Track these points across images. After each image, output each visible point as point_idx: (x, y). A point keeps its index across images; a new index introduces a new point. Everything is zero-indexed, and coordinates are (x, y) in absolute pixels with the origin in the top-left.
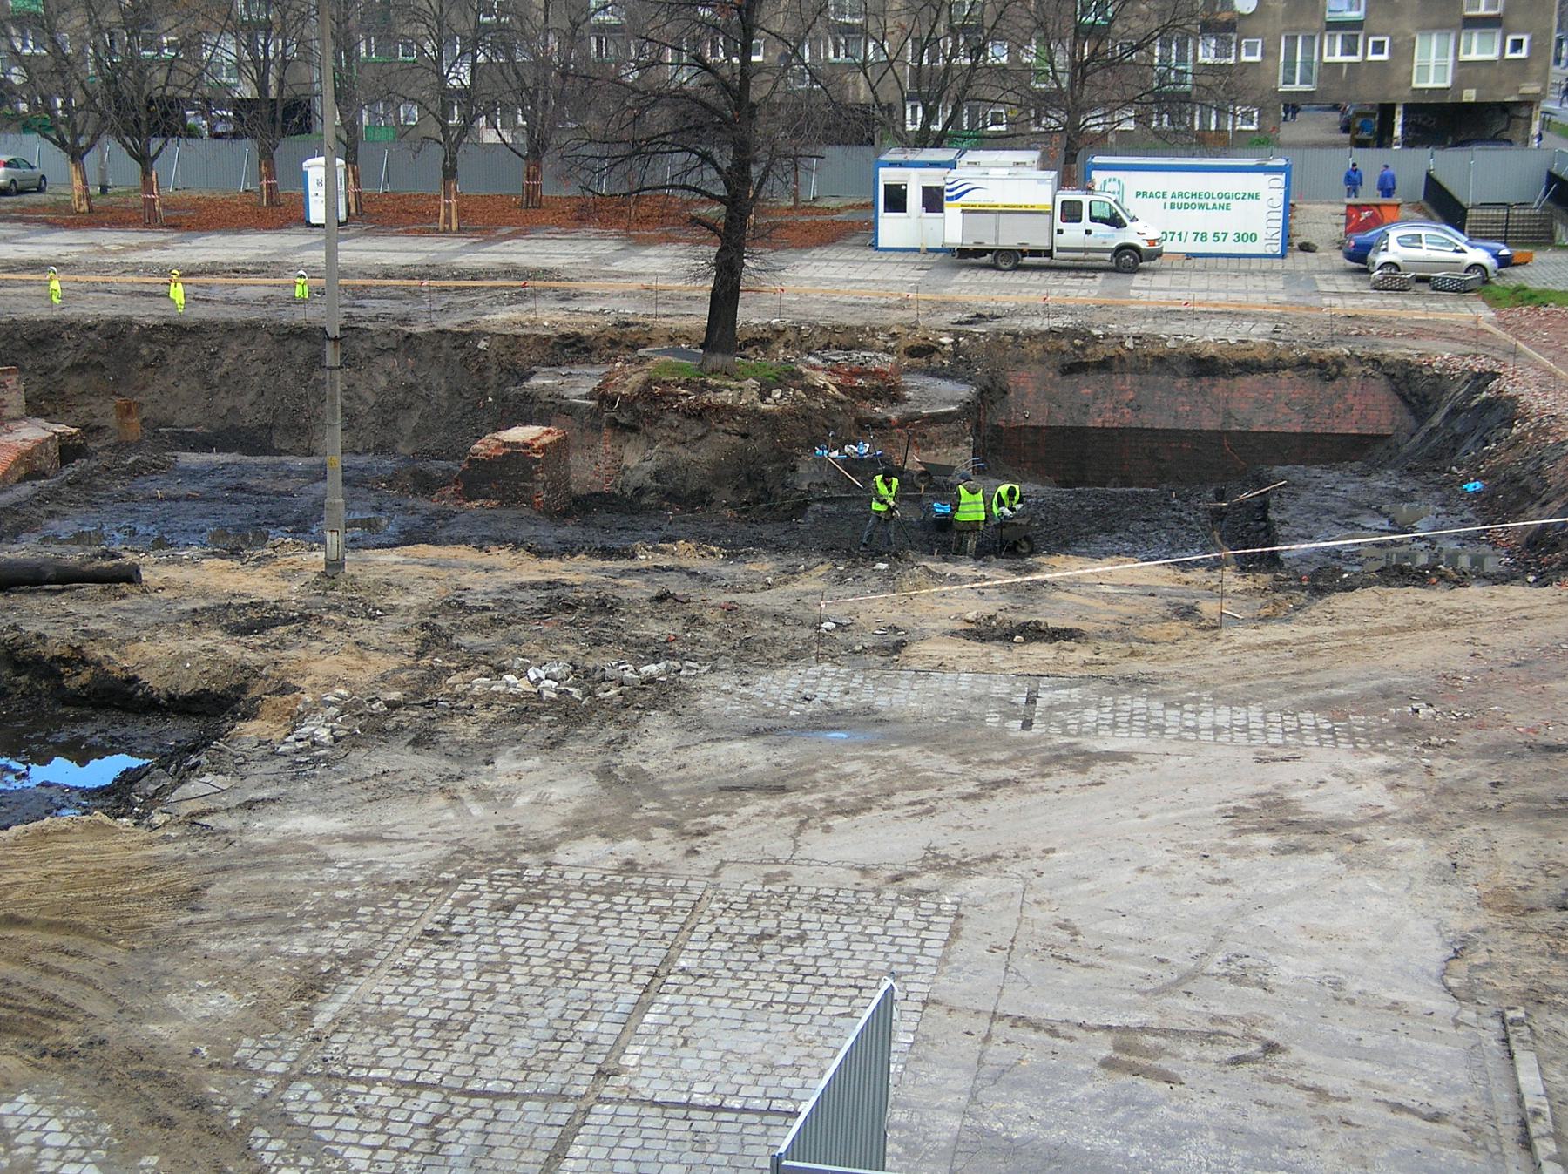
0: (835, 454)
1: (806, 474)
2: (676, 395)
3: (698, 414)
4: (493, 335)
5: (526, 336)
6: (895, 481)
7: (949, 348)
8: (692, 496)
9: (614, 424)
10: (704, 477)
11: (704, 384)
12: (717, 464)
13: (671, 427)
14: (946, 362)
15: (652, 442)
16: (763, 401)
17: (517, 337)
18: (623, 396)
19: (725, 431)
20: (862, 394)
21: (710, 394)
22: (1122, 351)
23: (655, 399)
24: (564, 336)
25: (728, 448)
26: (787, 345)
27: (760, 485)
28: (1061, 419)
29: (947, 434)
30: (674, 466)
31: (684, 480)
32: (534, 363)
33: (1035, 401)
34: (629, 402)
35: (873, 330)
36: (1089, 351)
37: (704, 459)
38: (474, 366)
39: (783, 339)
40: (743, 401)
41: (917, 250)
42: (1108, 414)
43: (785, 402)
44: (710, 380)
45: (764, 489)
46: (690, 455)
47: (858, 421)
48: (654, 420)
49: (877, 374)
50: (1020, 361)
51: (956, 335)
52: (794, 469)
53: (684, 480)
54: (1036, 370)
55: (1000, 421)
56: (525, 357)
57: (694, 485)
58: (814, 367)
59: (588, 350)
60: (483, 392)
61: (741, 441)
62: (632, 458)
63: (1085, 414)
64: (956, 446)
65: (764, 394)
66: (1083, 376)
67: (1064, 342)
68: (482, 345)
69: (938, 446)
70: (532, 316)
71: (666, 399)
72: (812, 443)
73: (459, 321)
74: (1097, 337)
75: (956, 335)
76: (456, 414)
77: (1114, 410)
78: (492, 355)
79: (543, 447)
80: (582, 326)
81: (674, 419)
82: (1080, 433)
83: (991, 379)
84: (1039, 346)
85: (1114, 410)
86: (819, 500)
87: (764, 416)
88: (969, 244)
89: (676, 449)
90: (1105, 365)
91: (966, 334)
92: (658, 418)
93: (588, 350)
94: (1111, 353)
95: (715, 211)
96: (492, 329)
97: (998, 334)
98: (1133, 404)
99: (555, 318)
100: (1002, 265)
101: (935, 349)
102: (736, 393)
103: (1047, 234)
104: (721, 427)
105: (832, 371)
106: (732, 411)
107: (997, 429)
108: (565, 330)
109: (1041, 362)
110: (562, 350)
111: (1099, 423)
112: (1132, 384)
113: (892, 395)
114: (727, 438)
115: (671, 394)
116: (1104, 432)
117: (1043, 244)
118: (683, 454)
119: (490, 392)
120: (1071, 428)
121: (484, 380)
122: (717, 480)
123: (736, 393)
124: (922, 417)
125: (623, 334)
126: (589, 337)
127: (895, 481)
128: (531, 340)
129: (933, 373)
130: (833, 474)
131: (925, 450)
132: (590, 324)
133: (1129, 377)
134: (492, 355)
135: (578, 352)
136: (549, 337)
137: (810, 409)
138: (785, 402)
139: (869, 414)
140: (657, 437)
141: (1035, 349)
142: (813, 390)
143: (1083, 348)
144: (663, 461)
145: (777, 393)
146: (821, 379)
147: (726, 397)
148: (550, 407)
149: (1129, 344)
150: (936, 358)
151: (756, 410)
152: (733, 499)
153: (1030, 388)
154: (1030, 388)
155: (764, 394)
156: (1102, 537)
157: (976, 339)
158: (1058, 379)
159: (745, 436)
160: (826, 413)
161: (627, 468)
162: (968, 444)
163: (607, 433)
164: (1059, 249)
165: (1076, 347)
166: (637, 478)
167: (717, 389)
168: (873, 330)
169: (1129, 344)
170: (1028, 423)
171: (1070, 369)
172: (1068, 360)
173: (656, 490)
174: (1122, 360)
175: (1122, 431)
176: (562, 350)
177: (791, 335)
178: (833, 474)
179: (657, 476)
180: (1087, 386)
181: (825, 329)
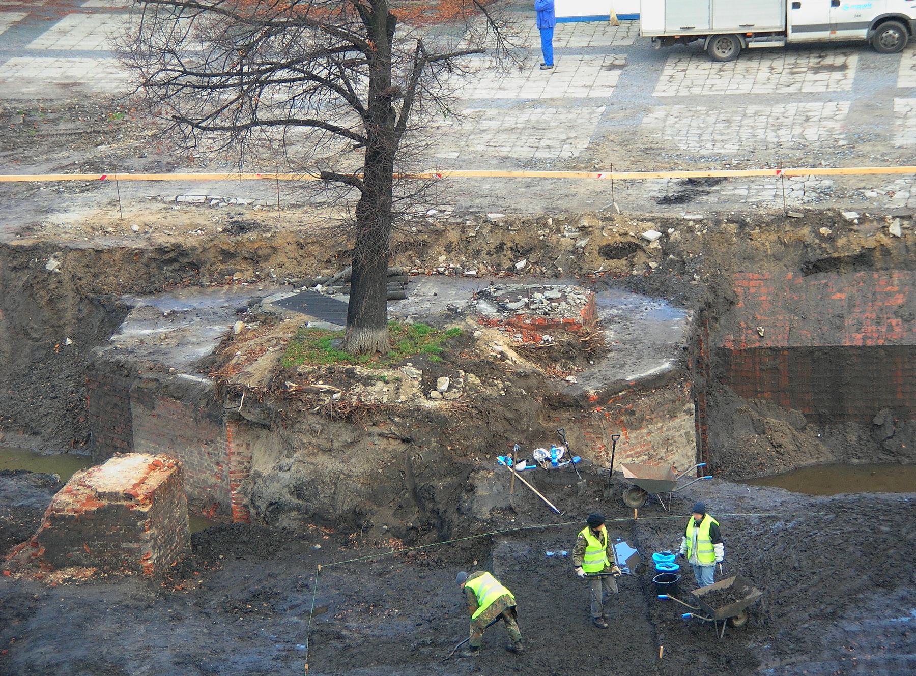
0: (522, 466)
1: (486, 498)
2: (317, 392)
3: (352, 416)
4: (66, 250)
5: (110, 251)
6: (604, 529)
7: (655, 245)
8: (343, 518)
9: (238, 419)
10: (358, 493)
11: (350, 374)
12: (373, 477)
13: (313, 432)
14: (653, 265)
15: (289, 448)
16: (426, 394)
17: (99, 252)
18: (249, 390)
19: (381, 435)
20: (547, 356)
21: (360, 388)
22: (886, 240)
23: (288, 398)
24: (161, 250)
25: (387, 456)
26: (449, 249)
27: (430, 506)
28: (807, 337)
29: (659, 404)
30: (317, 480)
31: (333, 497)
32: (125, 289)
33: (773, 313)
34: (256, 398)
35: (557, 222)
36: (841, 242)
37: (357, 470)
38: (43, 296)
39: (443, 241)
40: (403, 398)
41: (606, 18)
42: (871, 328)
43: (455, 394)
44: (358, 370)
45: (435, 512)
46: (340, 467)
47: (547, 400)
48: (289, 423)
49: (567, 326)
50: (750, 258)
51: (665, 225)
52: (472, 489)
53: (333, 497)
54: (771, 269)
55: (728, 341)
56: (114, 278)
57: (345, 504)
58: (487, 322)
59: (195, 266)
60: (58, 331)
61: (402, 447)
62: (264, 464)
63: (839, 328)
64: (673, 416)
65: (428, 386)
66: (833, 275)
67: (805, 231)
68: (53, 265)
69: (651, 421)
70: (115, 215)
71: (305, 397)
72: (494, 446)
73: (16, 224)
74: (851, 222)
75: (665, 225)
76: (23, 361)
77: (878, 321)
78: (66, 278)
79: (151, 497)
80: (184, 231)
81: (312, 421)
82: (834, 355)
83: (713, 290)
84: (773, 237)
85: (878, 321)
86: (505, 535)
87: (430, 418)
88: (675, 30)
89: (321, 459)
90: (863, 260)
91: (677, 223)
92: (295, 421)
93: (195, 266)
94: (871, 243)
95: (354, 163)
96: (64, 239)
97: (718, 222)
98: (905, 312)
99: (151, 219)
100: (719, 53)
101: (638, 247)
102: (392, 387)
103: (778, 11)
104: (376, 430)
105: (511, 325)
106: (389, 411)
107: (723, 353)
108: (163, 240)
109: (777, 258)
110: (160, 268)
111: (857, 340)
112: (902, 284)
113: (588, 351)
114: (383, 443)
115: (310, 391)
116: (866, 353)
117: (776, 24)
118: (329, 464)
119: (68, 330)
120: (820, 349)
121: (59, 313)
122: (374, 497)
123: (392, 387)
124: (628, 387)
125: (238, 243)
126: (194, 249)
127: (604, 529)
128: (117, 256)
129: (637, 287)
130: (521, 492)
131: (635, 429)
132: (195, 227)
133: (896, 274)
134: (66, 278)
135: (182, 269)
136: (142, 252)
137: (486, 399)
138: (455, 394)
139: (561, 388)
140: (295, 444)
141: (765, 241)
142: (490, 367)
143: (831, 239)
144: (305, 474)
145: (443, 383)
146: (499, 343)
147: (379, 393)
148: (152, 385)
149: (895, 229)
150: (640, 258)
151: (418, 409)
152: (396, 522)
153: (764, 294)
154: (764, 294)
155: (428, 386)
156: (877, 599)
157: (691, 230)
158: (800, 280)
159: (406, 441)
160: (507, 400)
161: (258, 475)
162: (689, 412)
163: (231, 429)
164: (797, 29)
165: (822, 238)
166: (273, 491)
167: (368, 381)
168: (557, 222)
169: (895, 229)
170: (764, 344)
171: (817, 266)
172: (812, 256)
173: (298, 508)
174: (885, 251)
175: (892, 351)
176: (160, 268)
177: (454, 236)
178: (521, 492)
179: (298, 491)
180: (840, 289)
181: (495, 225)
